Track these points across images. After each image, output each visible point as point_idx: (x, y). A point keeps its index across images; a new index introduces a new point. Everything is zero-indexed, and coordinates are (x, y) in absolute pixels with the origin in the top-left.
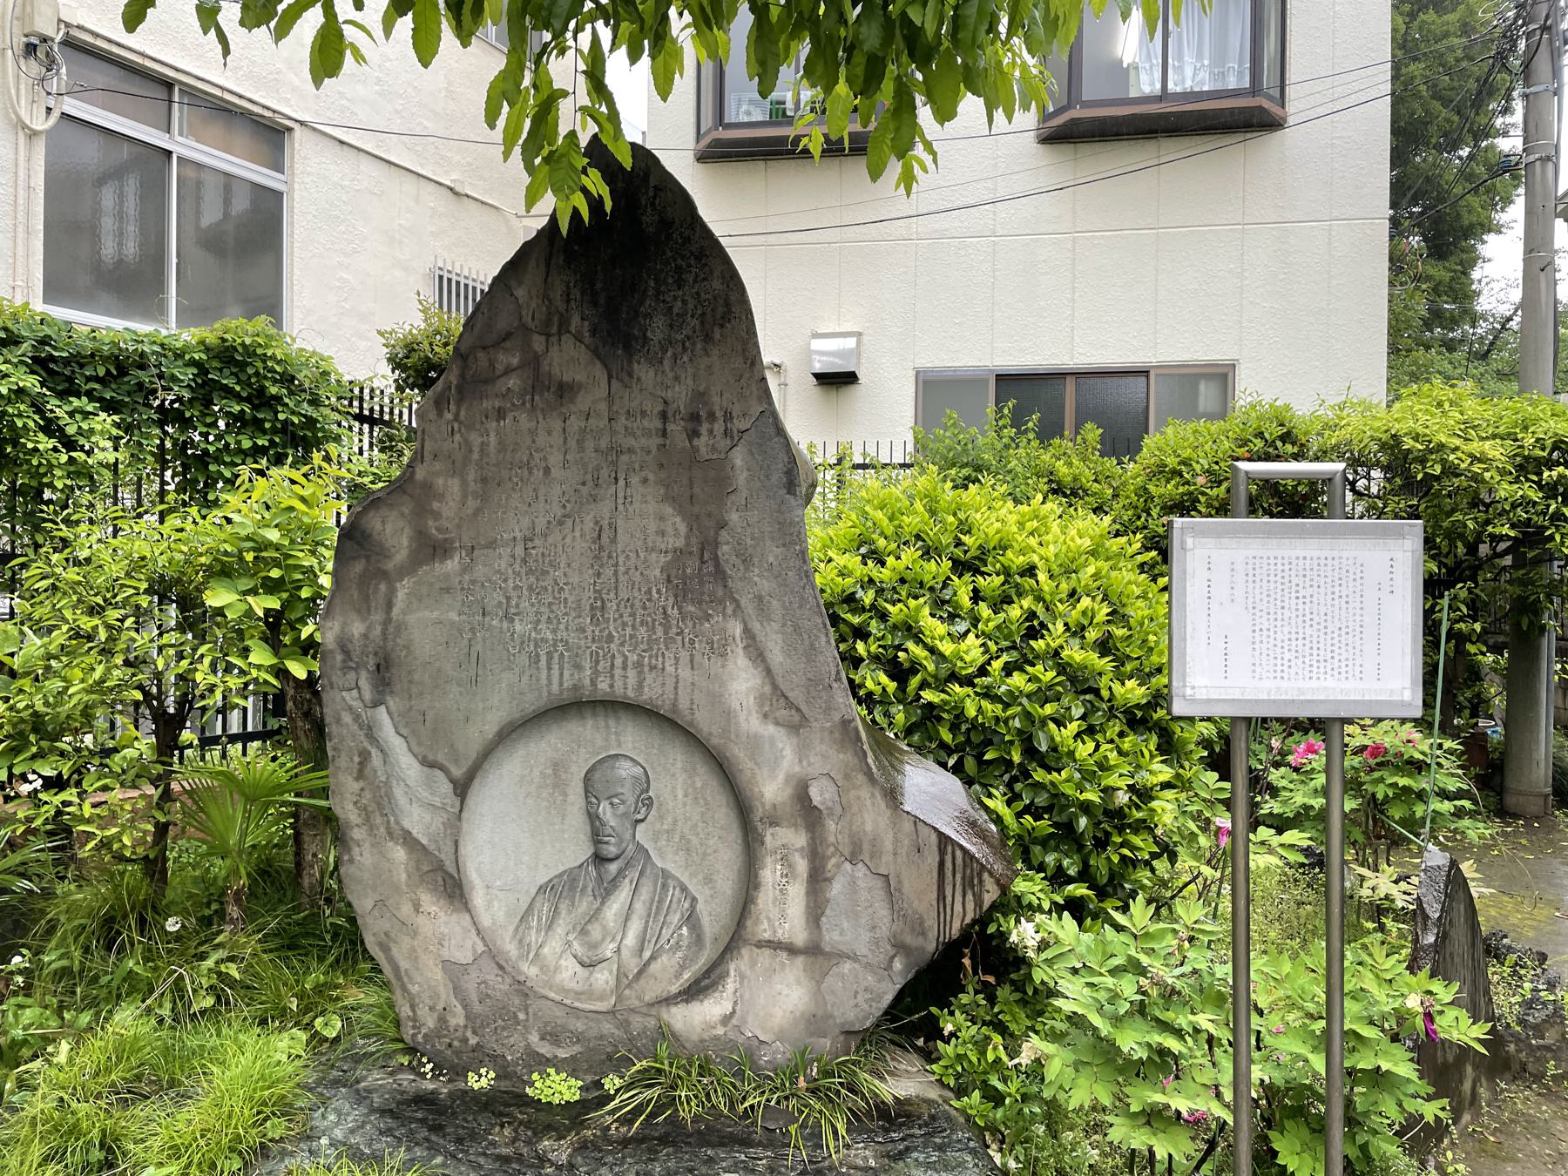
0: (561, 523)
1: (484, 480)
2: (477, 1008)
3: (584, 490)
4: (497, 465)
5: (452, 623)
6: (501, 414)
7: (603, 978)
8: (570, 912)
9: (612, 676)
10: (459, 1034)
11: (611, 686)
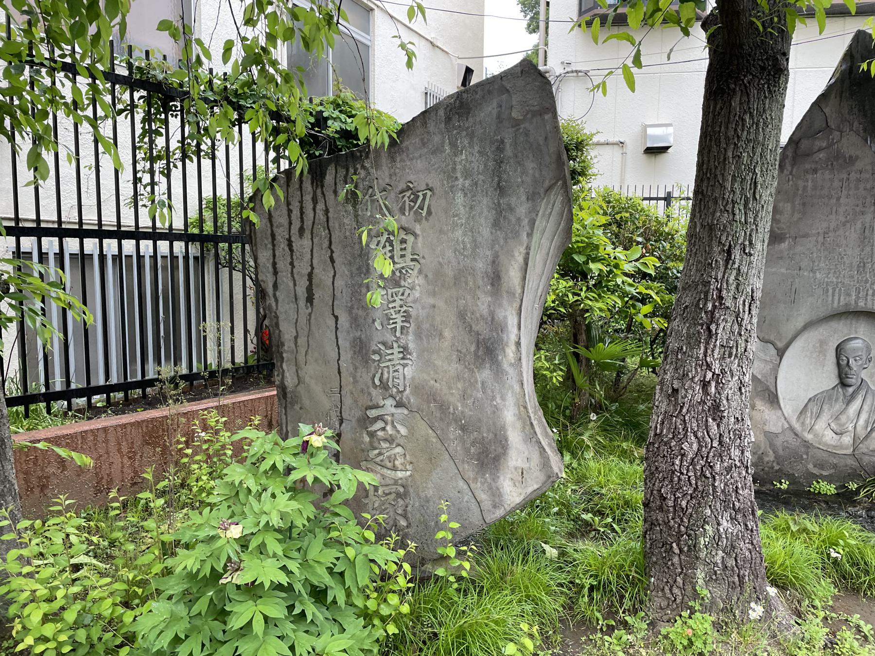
0: (844, 225)
1: (804, 204)
2: (781, 452)
3: (858, 209)
4: (811, 196)
5: (783, 274)
6: (815, 171)
7: (847, 439)
8: (829, 410)
9: (866, 300)
10: (770, 465)
11: (866, 304)
